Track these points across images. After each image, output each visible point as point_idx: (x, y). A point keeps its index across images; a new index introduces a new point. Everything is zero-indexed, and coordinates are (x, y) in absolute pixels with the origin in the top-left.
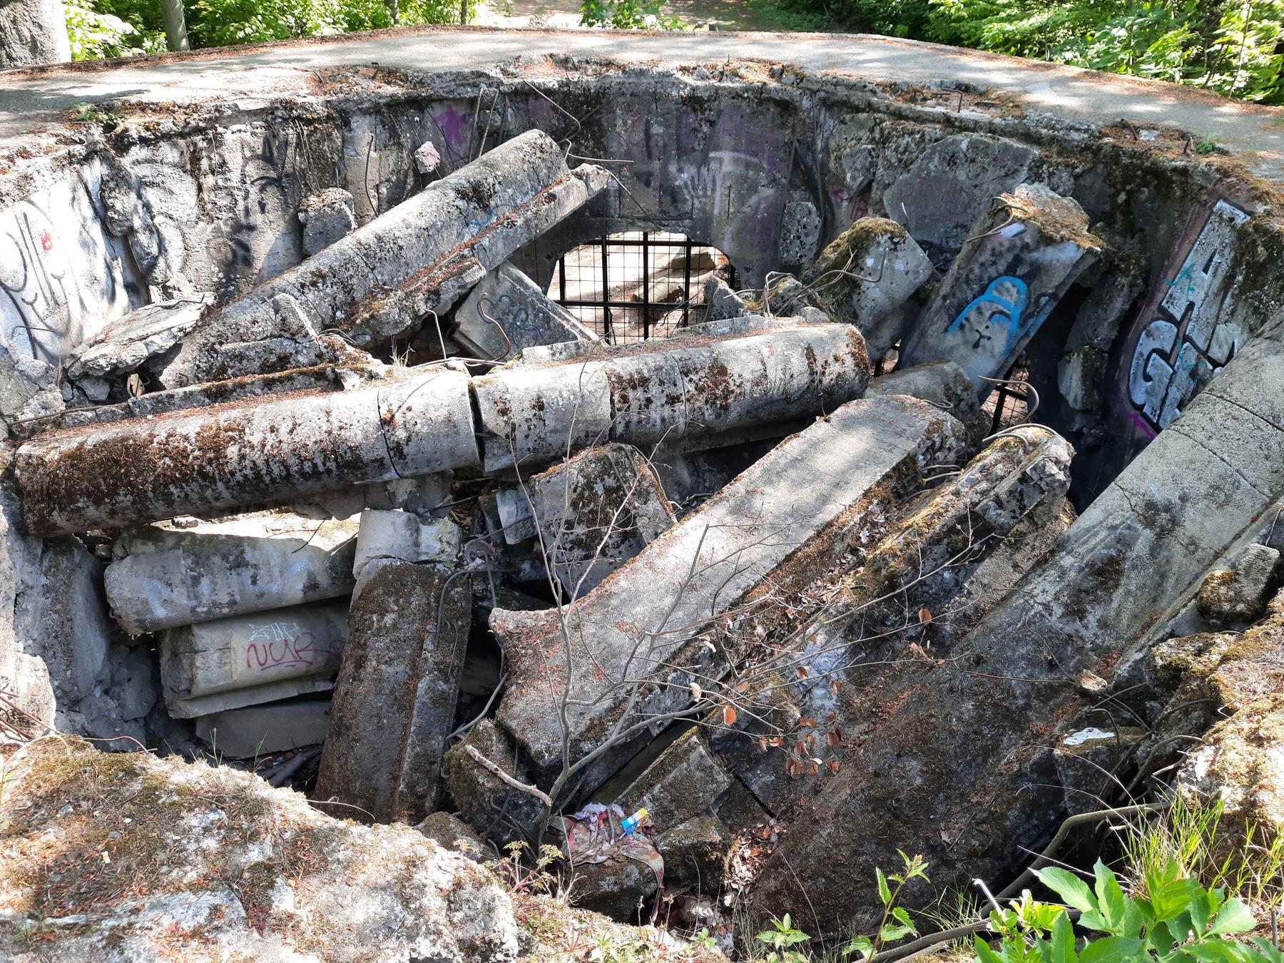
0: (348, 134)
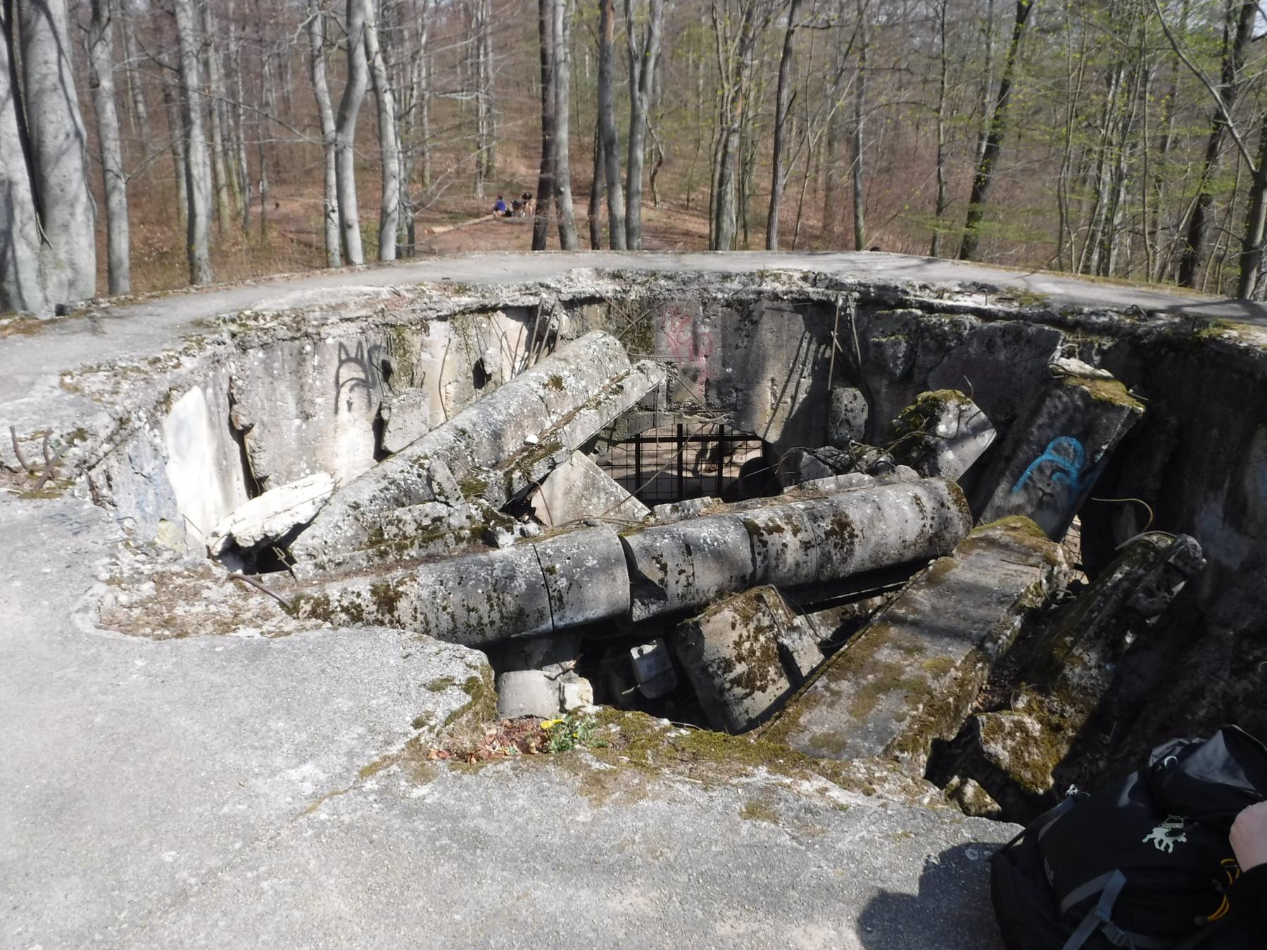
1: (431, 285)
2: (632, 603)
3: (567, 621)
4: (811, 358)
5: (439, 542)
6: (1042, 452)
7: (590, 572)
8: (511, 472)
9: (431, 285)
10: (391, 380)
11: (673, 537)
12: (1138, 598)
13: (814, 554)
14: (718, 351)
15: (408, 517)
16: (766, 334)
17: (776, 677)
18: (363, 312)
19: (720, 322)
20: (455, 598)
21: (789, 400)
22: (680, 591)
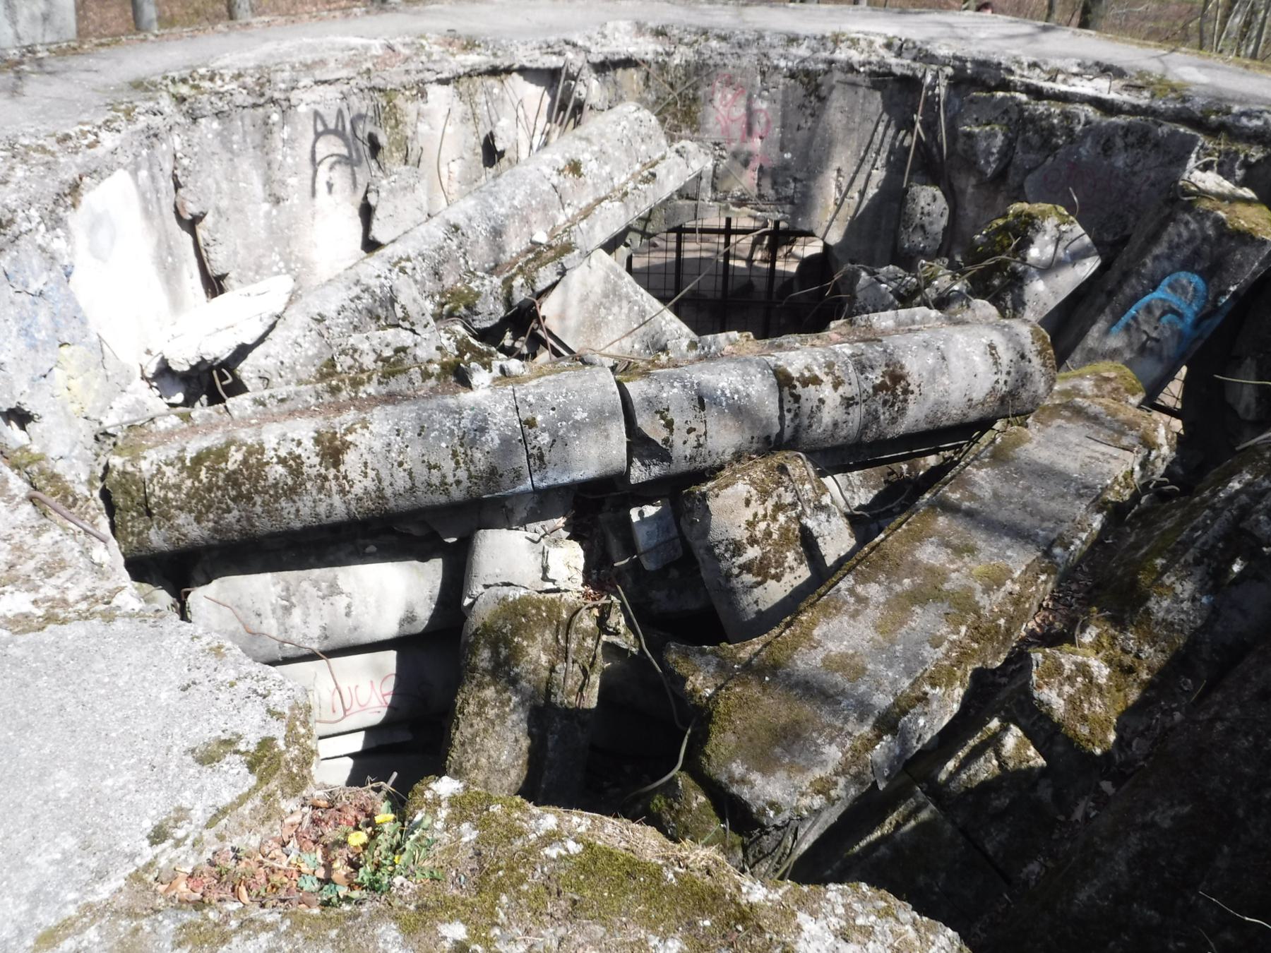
0: (424, 107)
1: (434, 37)
2: (630, 462)
3: (550, 482)
4: (886, 146)
5: (402, 379)
6: (1154, 288)
7: (578, 426)
8: (512, 278)
9: (434, 37)
10: (380, 157)
11: (684, 386)
12: (1258, 521)
13: (857, 413)
14: (776, 132)
15: (365, 346)
16: (836, 113)
17: (795, 564)
18: (343, 73)
19: (780, 97)
20: (413, 452)
21: (856, 195)
22: (688, 453)
